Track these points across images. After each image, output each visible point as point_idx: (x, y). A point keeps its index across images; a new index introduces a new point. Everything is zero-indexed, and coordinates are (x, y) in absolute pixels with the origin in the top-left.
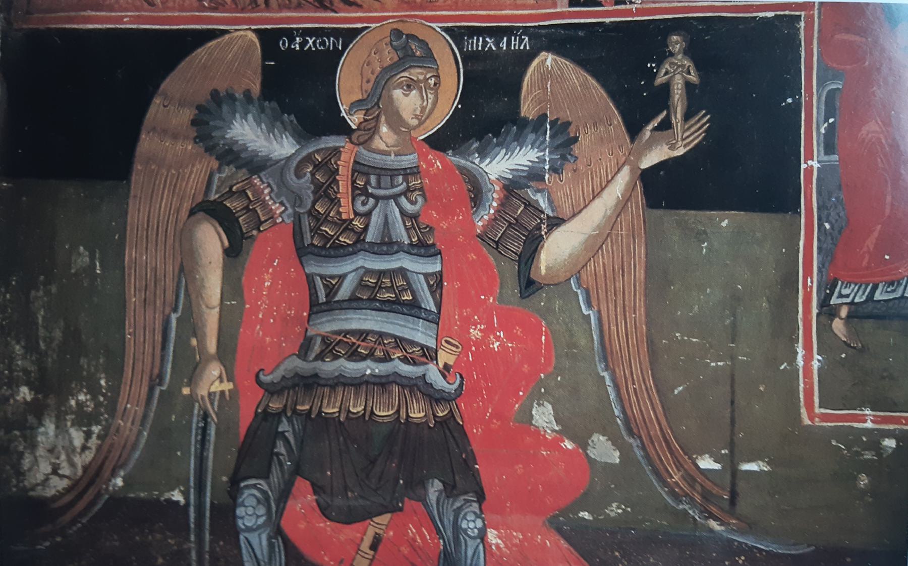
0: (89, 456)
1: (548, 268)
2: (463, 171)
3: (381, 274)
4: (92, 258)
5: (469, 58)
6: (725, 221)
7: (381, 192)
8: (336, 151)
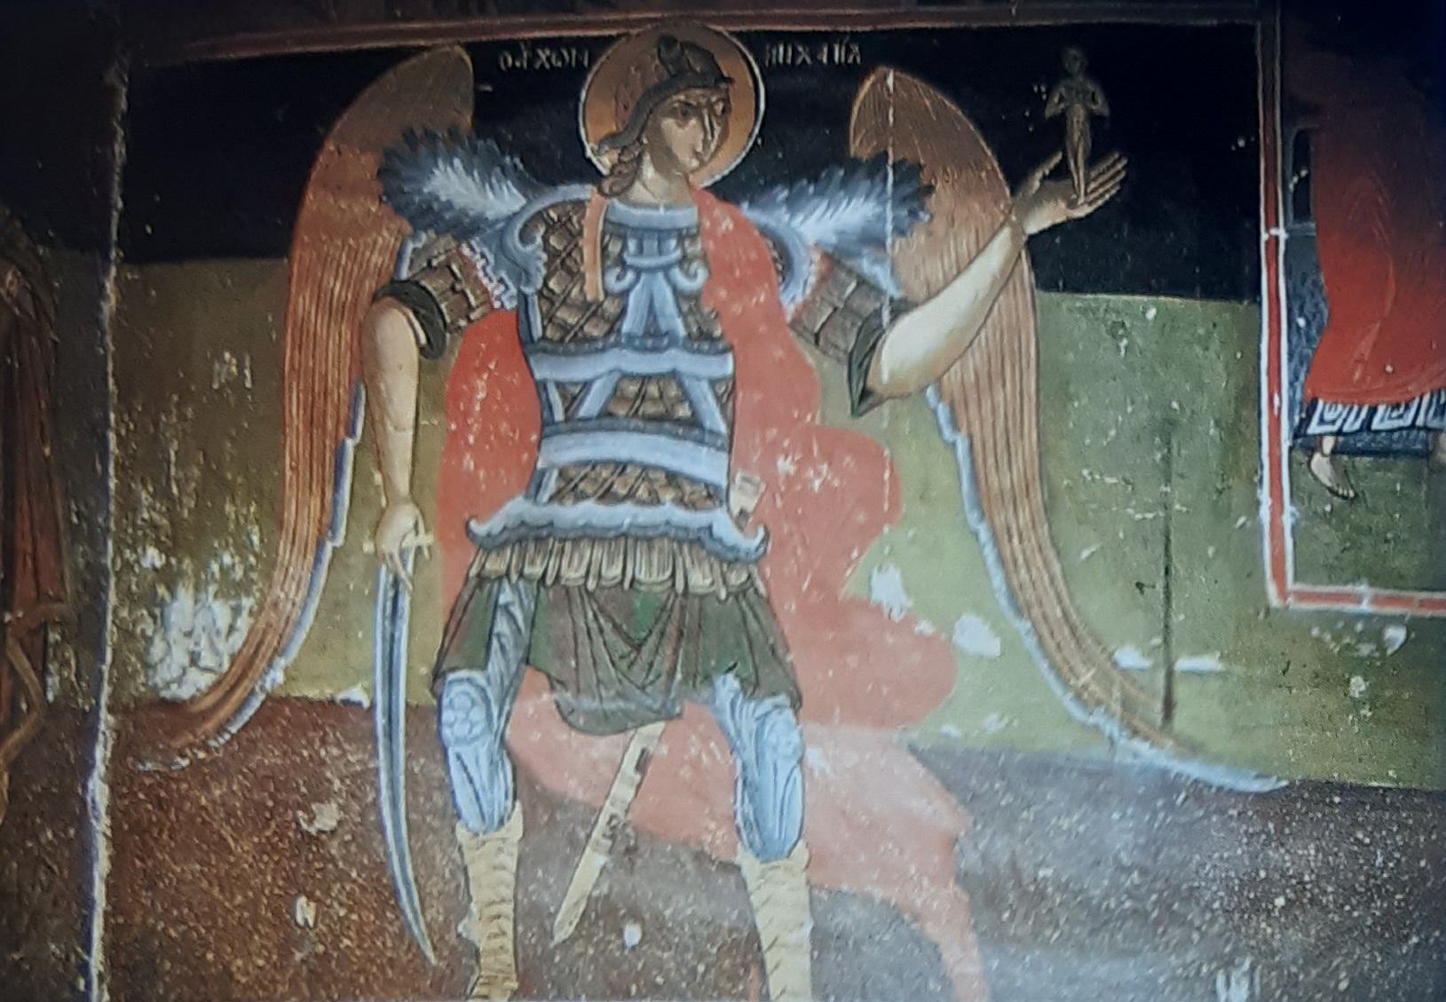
0: (238, 640)
1: (892, 375)
2: (765, 232)
3: (645, 379)
4: (240, 367)
5: (771, 72)
6: (1150, 307)
7: (645, 262)
8: (580, 205)
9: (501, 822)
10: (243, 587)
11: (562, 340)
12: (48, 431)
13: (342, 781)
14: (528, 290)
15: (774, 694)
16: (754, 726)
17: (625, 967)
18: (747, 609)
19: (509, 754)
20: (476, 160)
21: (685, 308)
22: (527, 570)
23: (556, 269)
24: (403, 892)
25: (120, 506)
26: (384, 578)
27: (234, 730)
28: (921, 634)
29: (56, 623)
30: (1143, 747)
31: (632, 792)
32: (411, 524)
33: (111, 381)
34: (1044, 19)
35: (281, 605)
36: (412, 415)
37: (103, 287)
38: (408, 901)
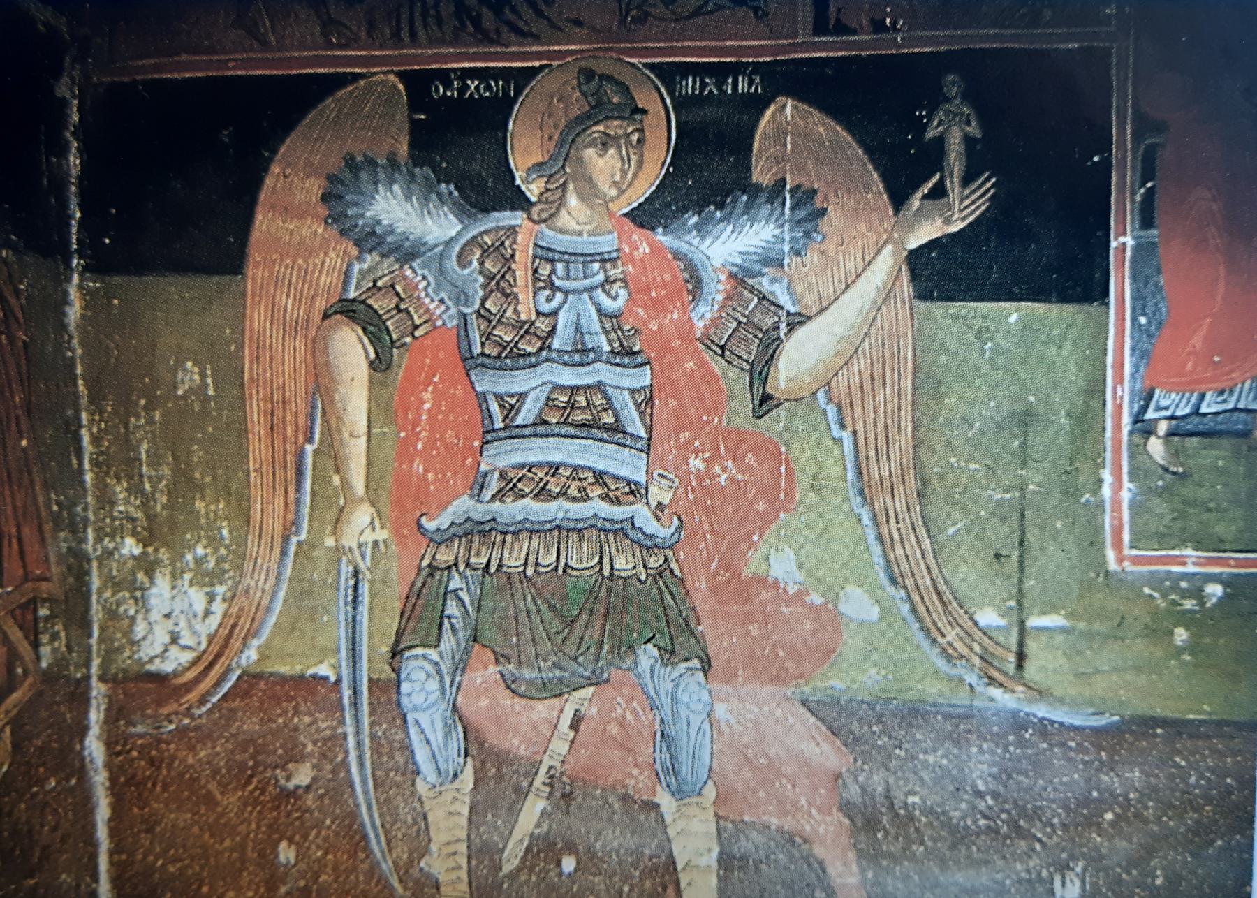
0: (214, 622)
2: (678, 255)
3: (575, 390)
4: (203, 375)
6: (1013, 313)
8: (512, 230)
9: (455, 776)
10: (215, 577)
11: (498, 357)
12: (24, 427)
13: (315, 743)
14: (467, 310)
15: (687, 660)
16: (670, 686)
17: (563, 890)
18: (663, 588)
19: (460, 718)
20: (414, 187)
21: (608, 325)
22: (473, 560)
23: (492, 292)
24: (372, 835)
25: (98, 499)
26: (346, 570)
27: (214, 700)
28: (813, 605)
29: (45, 600)
30: (996, 692)
31: (567, 747)
32: (367, 520)
33: (80, 382)
34: (925, 46)
35: (251, 592)
36: (365, 423)
37: (66, 293)
38: (377, 846)
